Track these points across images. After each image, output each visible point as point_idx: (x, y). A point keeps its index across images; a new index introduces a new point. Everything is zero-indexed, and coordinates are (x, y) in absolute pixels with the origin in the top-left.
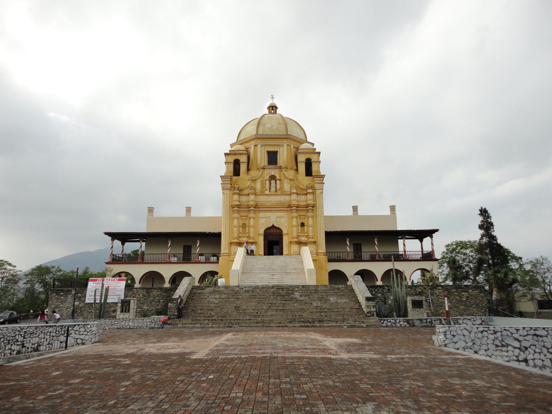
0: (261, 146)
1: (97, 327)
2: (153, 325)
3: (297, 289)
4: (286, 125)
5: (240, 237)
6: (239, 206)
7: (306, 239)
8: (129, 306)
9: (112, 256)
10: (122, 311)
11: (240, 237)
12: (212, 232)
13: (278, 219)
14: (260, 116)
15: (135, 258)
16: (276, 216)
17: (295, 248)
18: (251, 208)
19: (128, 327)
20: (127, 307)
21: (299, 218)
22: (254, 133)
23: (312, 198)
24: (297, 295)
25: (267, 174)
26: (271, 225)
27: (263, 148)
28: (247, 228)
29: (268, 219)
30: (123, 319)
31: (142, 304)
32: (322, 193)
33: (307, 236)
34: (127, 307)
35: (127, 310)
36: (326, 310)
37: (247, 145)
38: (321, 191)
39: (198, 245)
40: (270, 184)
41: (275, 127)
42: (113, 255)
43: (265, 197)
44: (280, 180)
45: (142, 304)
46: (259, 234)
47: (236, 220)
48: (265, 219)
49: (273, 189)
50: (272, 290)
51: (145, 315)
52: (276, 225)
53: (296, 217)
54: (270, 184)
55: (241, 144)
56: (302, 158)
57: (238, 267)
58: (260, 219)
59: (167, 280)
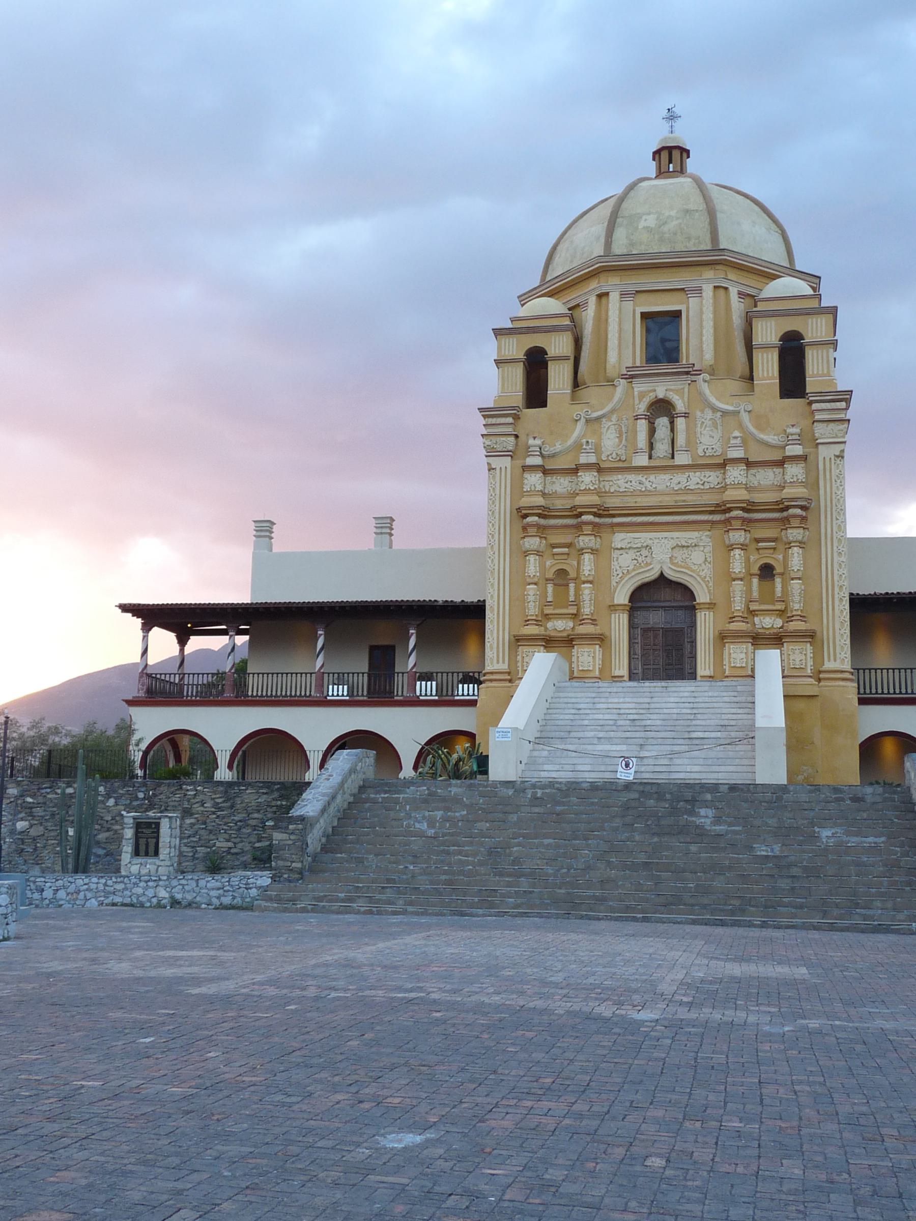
0: (623, 295)
1: (11, 896)
2: (227, 900)
3: (709, 797)
4: (712, 213)
5: (753, 613)
6: (544, 513)
7: (779, 623)
8: (157, 838)
9: (145, 680)
10: (137, 853)
11: (753, 613)
12: (458, 599)
13: (679, 555)
14: (619, 190)
15: (226, 689)
16: (673, 543)
17: (737, 653)
18: (585, 518)
19: (155, 900)
20: (152, 842)
21: (754, 546)
22: (599, 250)
23: (802, 477)
24: (705, 817)
25: (642, 395)
26: (652, 575)
27: (629, 305)
28: (572, 586)
29: (644, 552)
30: (139, 876)
31: (211, 832)
32: (841, 456)
33: (781, 613)
34: (152, 842)
35: (152, 849)
36: (795, 871)
37: (573, 297)
38: (836, 449)
39: (412, 642)
40: (652, 431)
41: (672, 225)
42: (149, 676)
43: (633, 477)
44: (686, 415)
45: (211, 832)
46: (613, 608)
47: (532, 558)
48: (632, 554)
49: (662, 448)
50: (625, 797)
51: (215, 868)
52: (671, 574)
53: (744, 547)
54: (652, 431)
55: (551, 294)
56: (768, 333)
57: (542, 716)
58: (615, 554)
59: (223, 760)
